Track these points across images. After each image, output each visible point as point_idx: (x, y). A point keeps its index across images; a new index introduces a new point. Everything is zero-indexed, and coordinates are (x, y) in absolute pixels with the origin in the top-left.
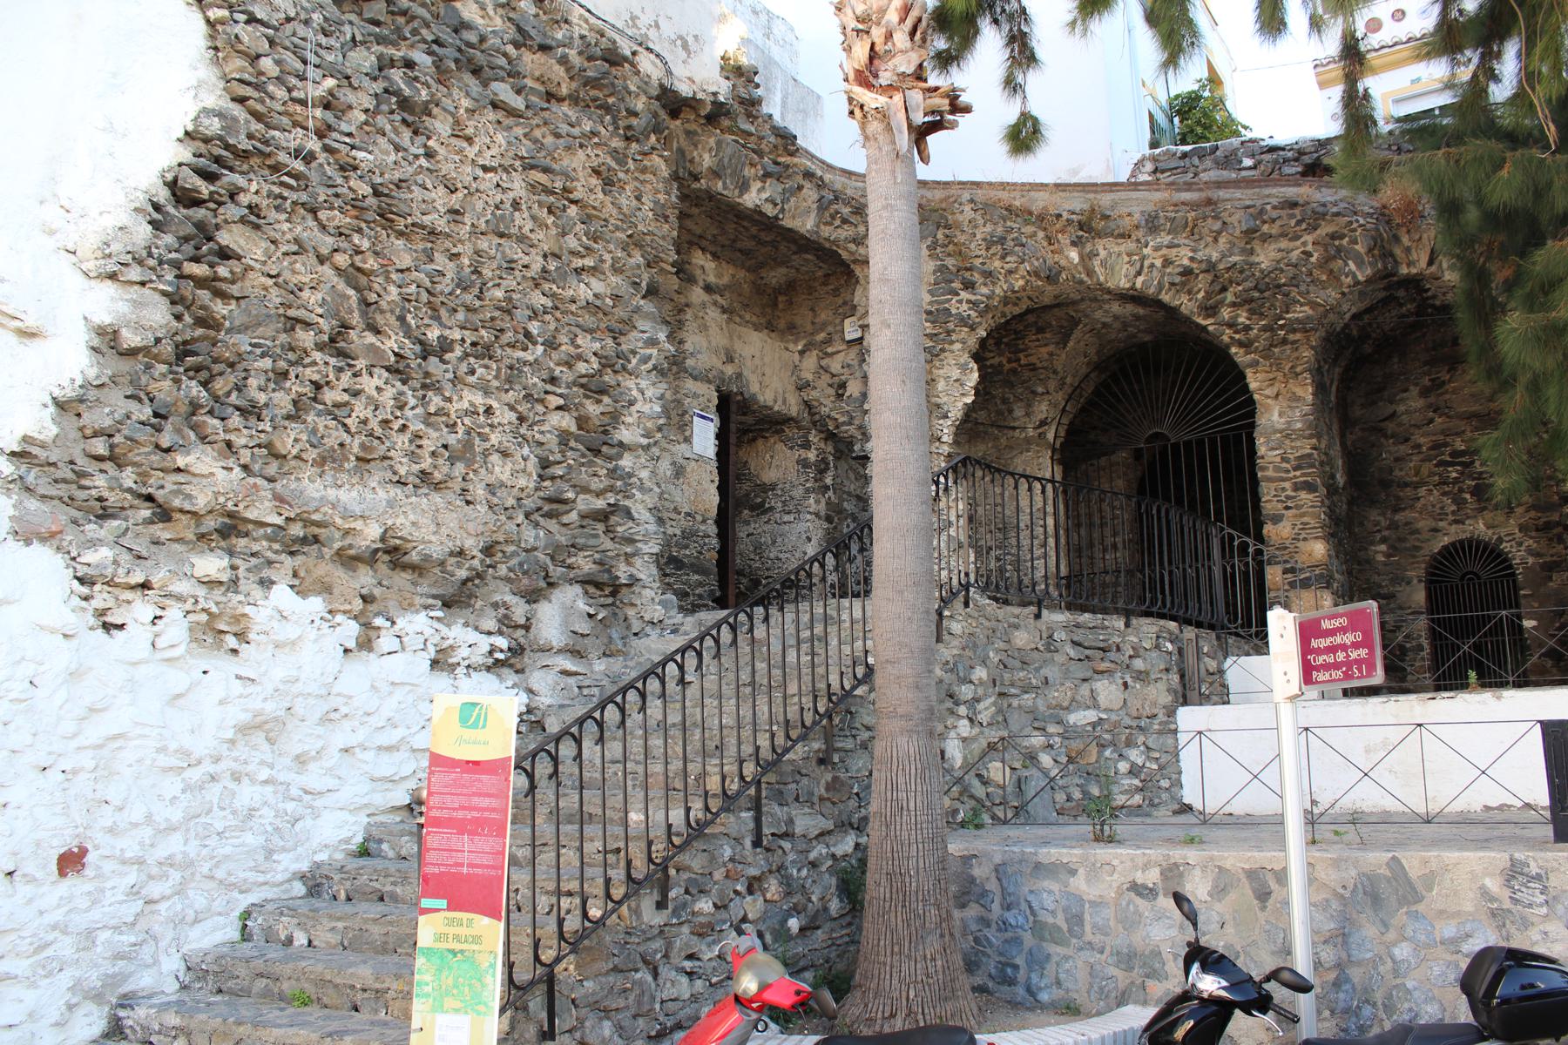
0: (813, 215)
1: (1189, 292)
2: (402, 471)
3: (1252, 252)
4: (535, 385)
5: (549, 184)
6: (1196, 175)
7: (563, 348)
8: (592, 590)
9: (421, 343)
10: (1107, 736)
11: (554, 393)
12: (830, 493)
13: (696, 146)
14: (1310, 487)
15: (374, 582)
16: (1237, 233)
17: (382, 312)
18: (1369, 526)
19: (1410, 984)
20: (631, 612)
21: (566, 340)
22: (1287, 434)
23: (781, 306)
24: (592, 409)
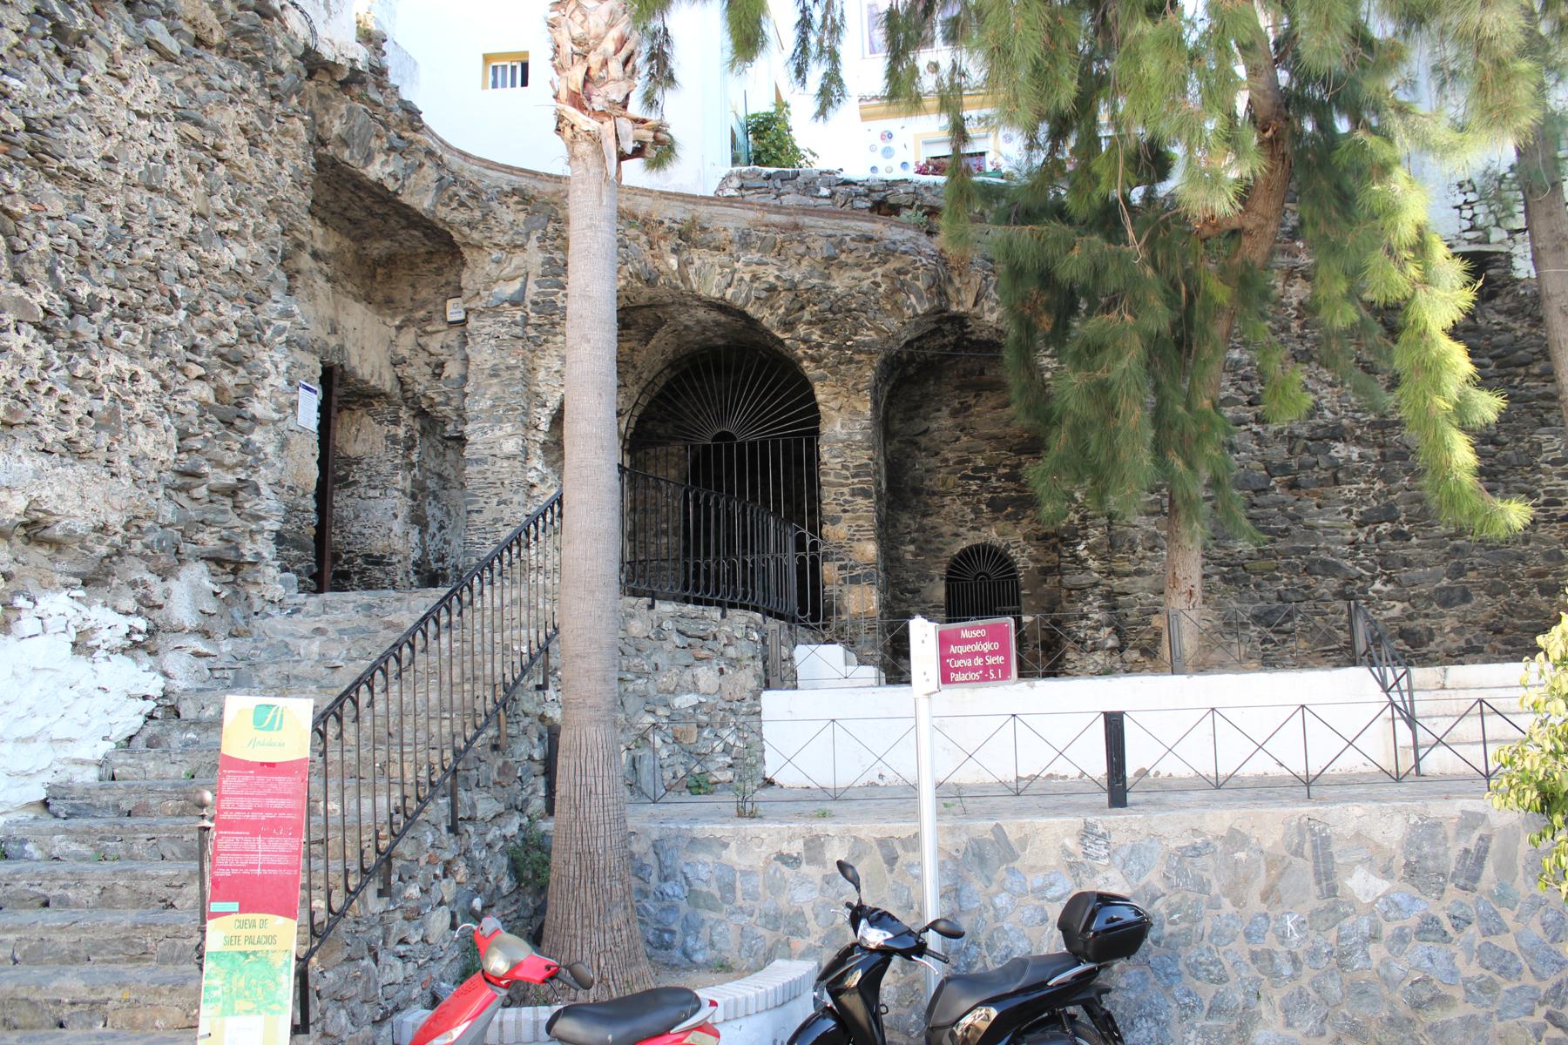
0: (431, 194)
2: (49, 438)
3: (829, 277)
4: (178, 352)
5: (200, 139)
6: (778, 196)
7: (206, 314)
8: (214, 567)
9: (70, 299)
10: (705, 718)
11: (194, 362)
12: (416, 470)
13: (327, 111)
14: (865, 494)
15: (11, 557)
16: (819, 258)
17: (31, 262)
18: (901, 527)
19: (1006, 927)
20: (253, 591)
21: (209, 307)
22: (848, 445)
23: (379, 278)
24: (228, 380)
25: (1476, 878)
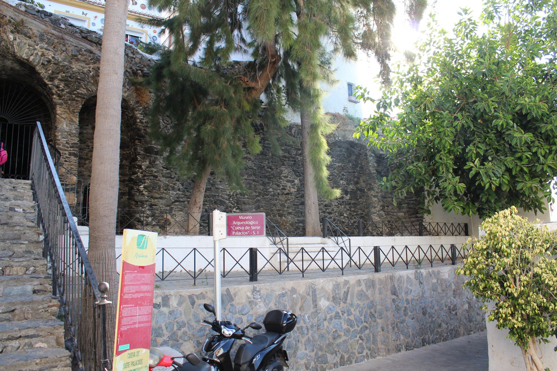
1: (46, 69)
14: (75, 155)
16: (70, 54)
25: (346, 300)
